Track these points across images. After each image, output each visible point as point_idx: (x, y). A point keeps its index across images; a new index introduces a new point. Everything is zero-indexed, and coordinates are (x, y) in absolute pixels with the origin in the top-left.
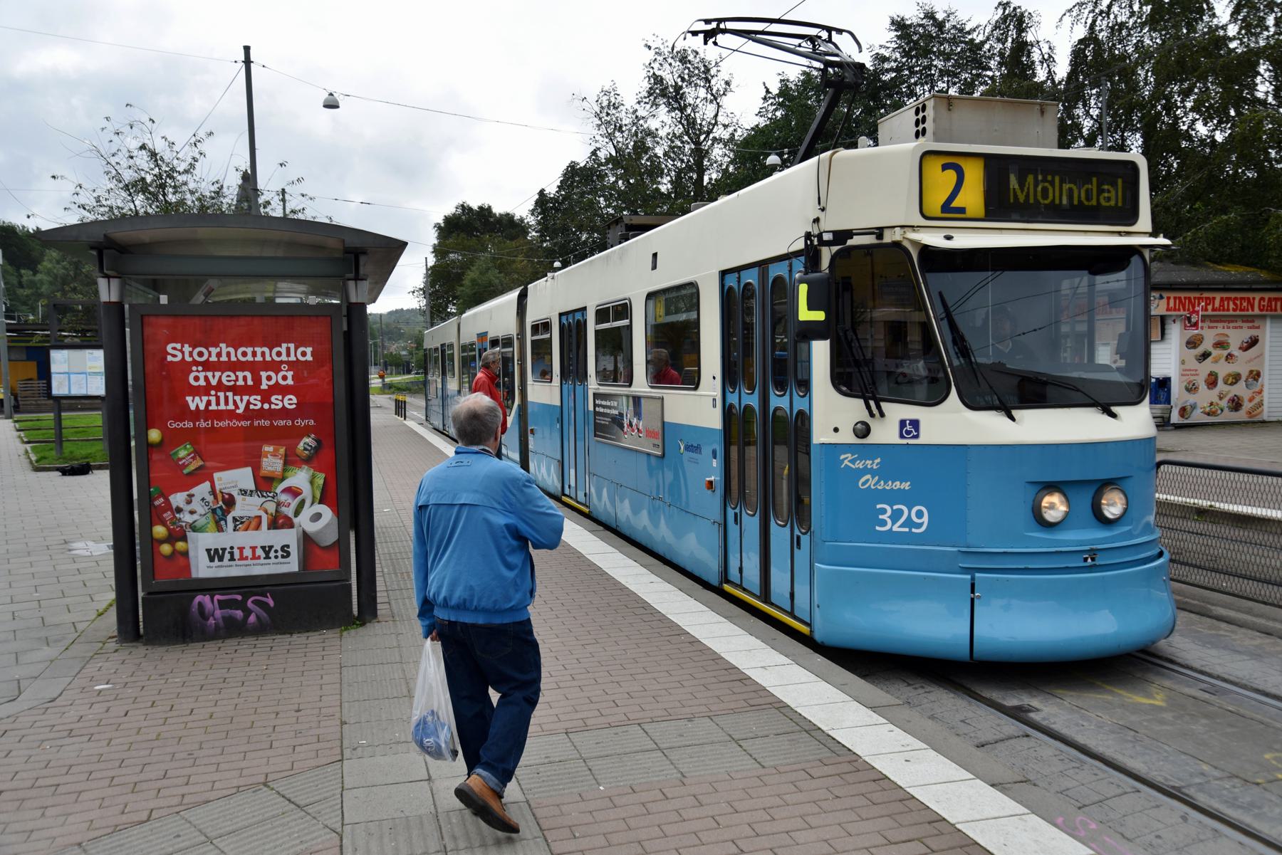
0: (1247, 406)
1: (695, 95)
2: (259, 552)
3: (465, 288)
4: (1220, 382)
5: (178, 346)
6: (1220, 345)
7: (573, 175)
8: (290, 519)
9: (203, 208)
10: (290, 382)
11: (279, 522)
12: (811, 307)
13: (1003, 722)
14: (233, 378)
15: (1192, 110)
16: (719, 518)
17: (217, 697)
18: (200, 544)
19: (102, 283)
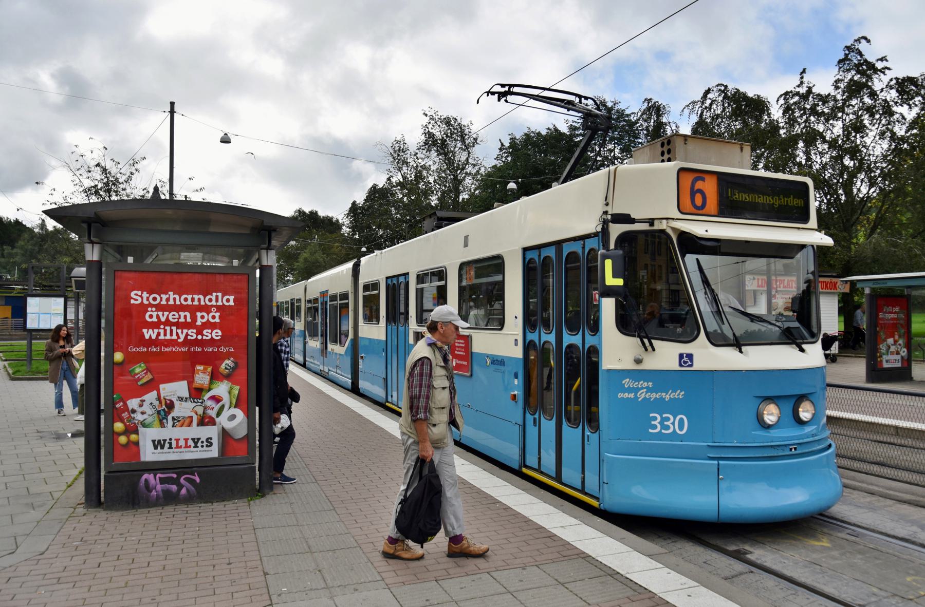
1: (455, 146)
2: (190, 443)
3: (299, 264)
5: (139, 293)
7: (374, 192)
10: (217, 320)
11: (206, 420)
12: (615, 276)
14: (177, 316)
16: (520, 422)
17: (166, 552)
18: (147, 436)
19: (88, 247)
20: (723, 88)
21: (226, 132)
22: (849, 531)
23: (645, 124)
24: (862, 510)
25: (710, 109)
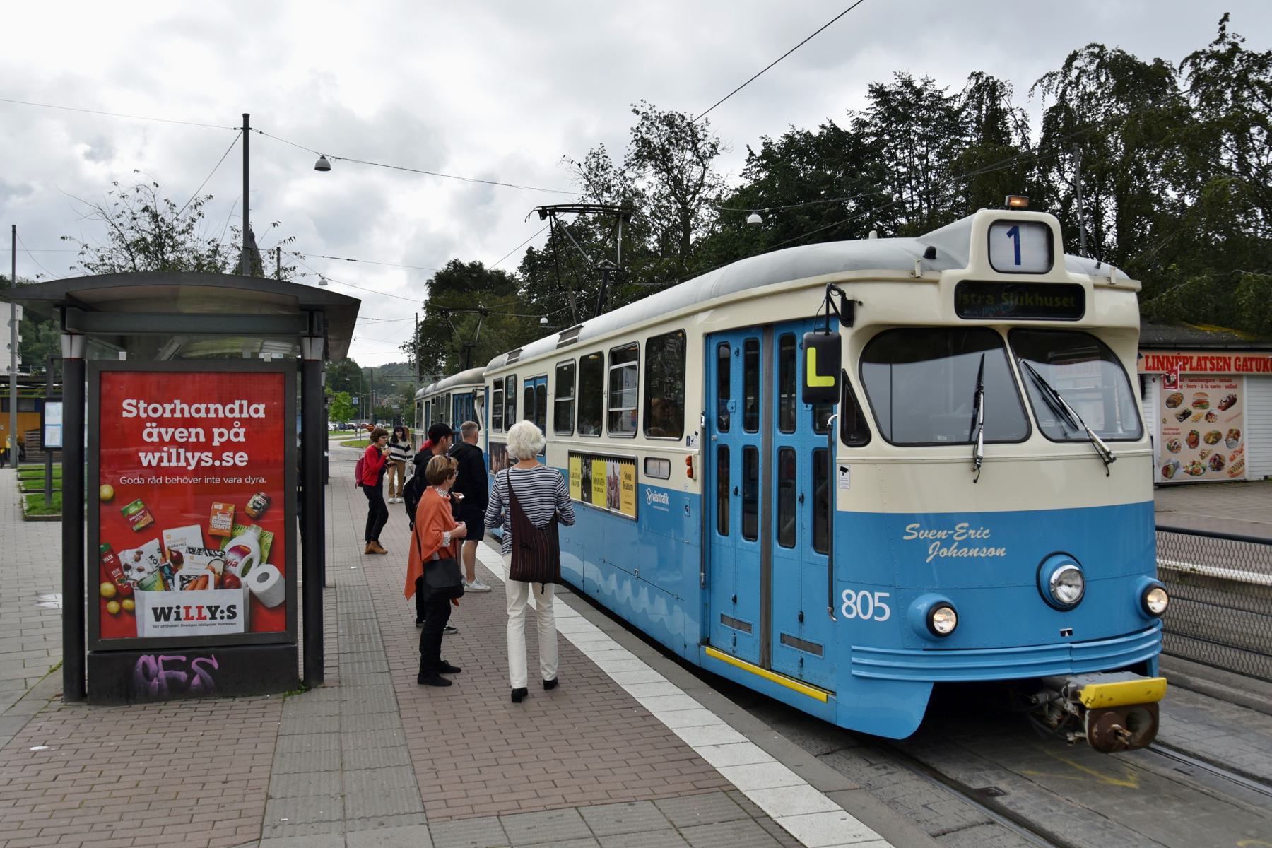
0: (1228, 465)
2: (205, 612)
4: (1201, 441)
5: (134, 402)
6: (1200, 404)
8: (237, 579)
9: (199, 266)
10: (242, 439)
13: (966, 808)
14: (186, 434)
15: (1162, 174)
18: (147, 602)
19: (65, 339)
20: (1096, 50)
21: (323, 153)
22: (1178, 765)
23: (975, 114)
24: (1214, 732)
25: (1077, 85)
